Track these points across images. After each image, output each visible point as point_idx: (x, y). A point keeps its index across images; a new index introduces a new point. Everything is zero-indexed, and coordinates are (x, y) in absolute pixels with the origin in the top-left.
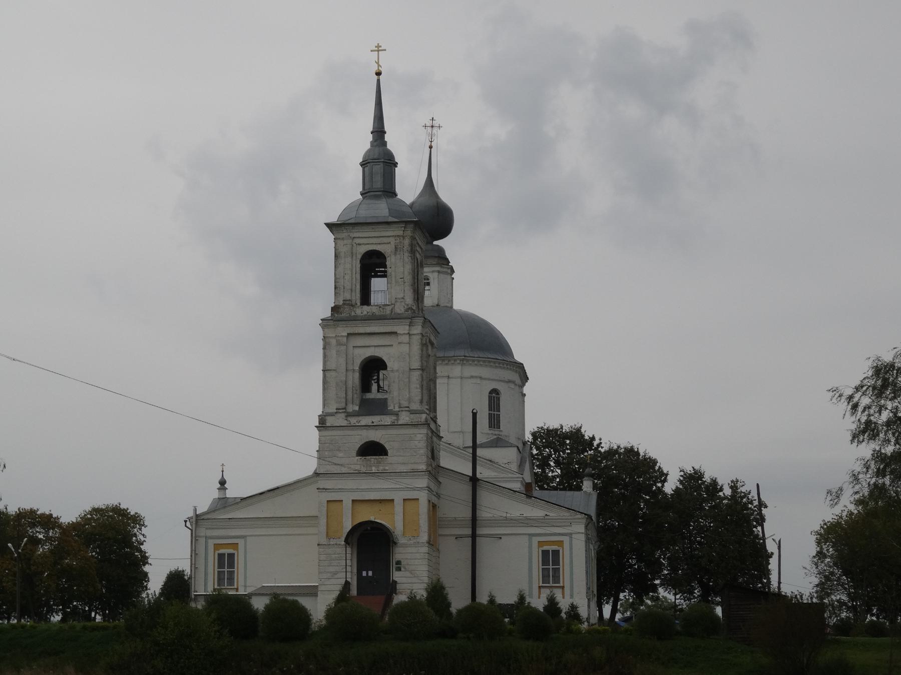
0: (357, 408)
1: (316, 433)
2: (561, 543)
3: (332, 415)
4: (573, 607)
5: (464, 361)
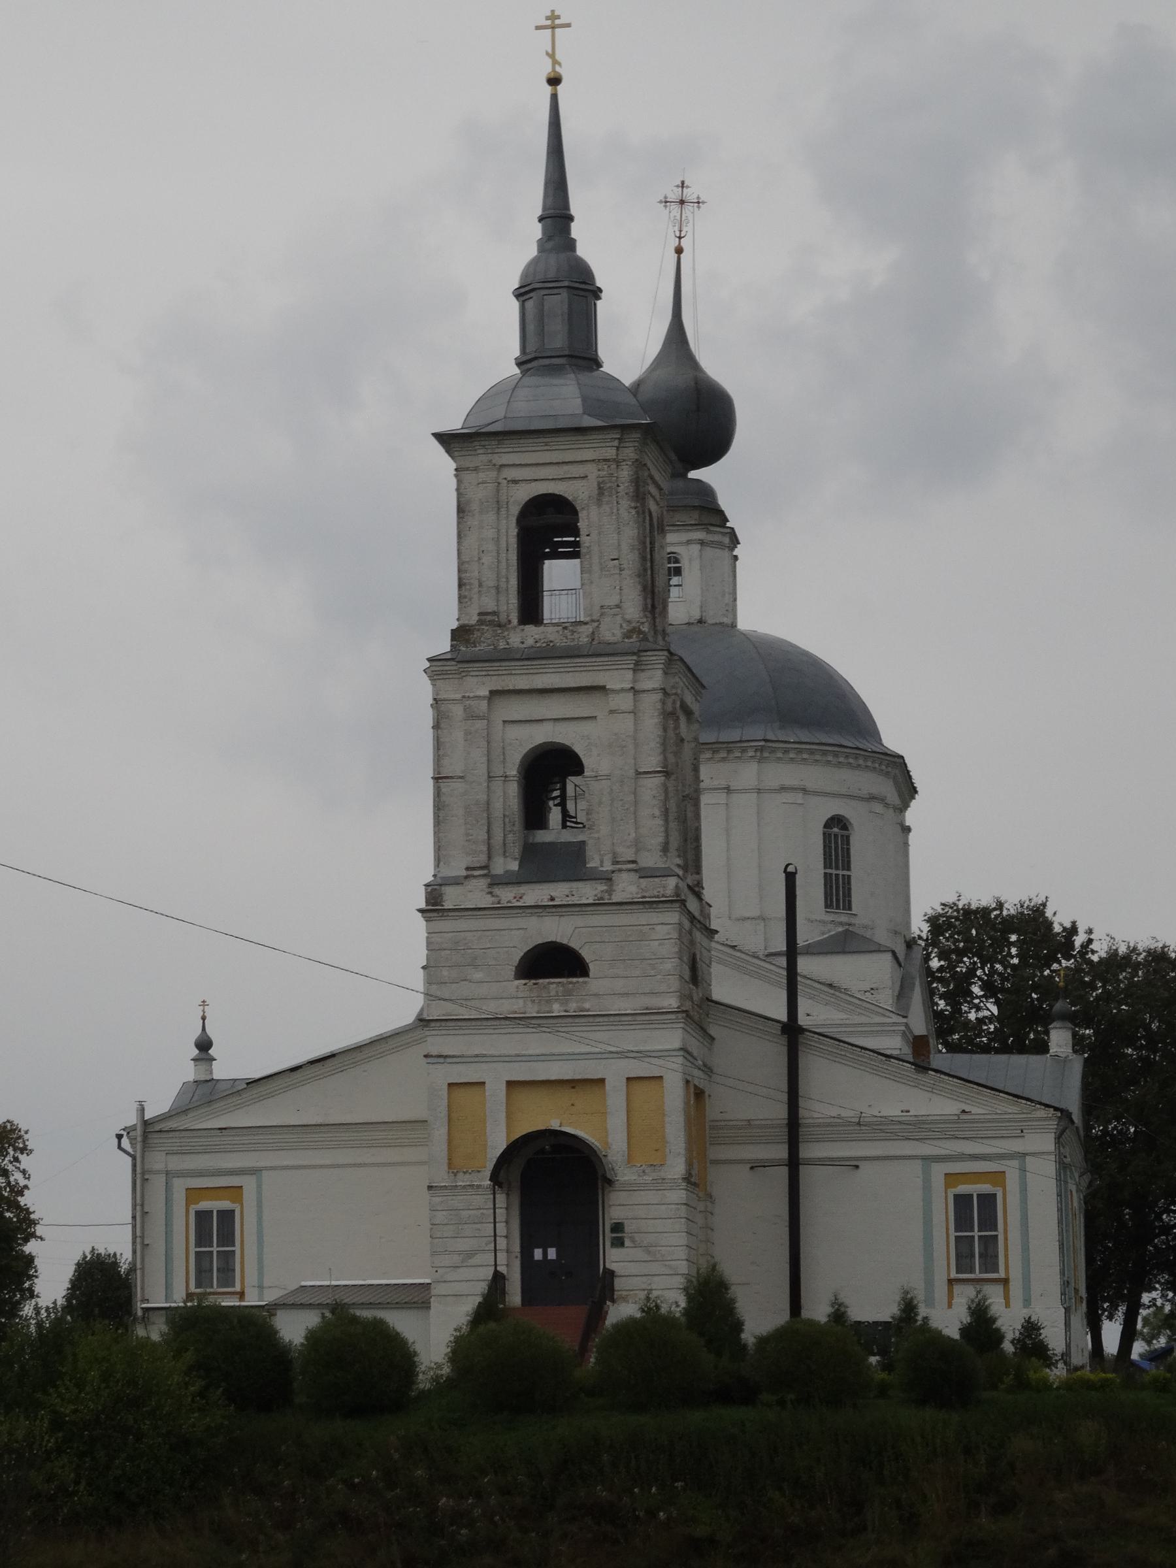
0: (514, 866)
1: (419, 927)
2: (998, 1178)
3: (456, 882)
4: (1031, 1328)
5: (764, 751)
